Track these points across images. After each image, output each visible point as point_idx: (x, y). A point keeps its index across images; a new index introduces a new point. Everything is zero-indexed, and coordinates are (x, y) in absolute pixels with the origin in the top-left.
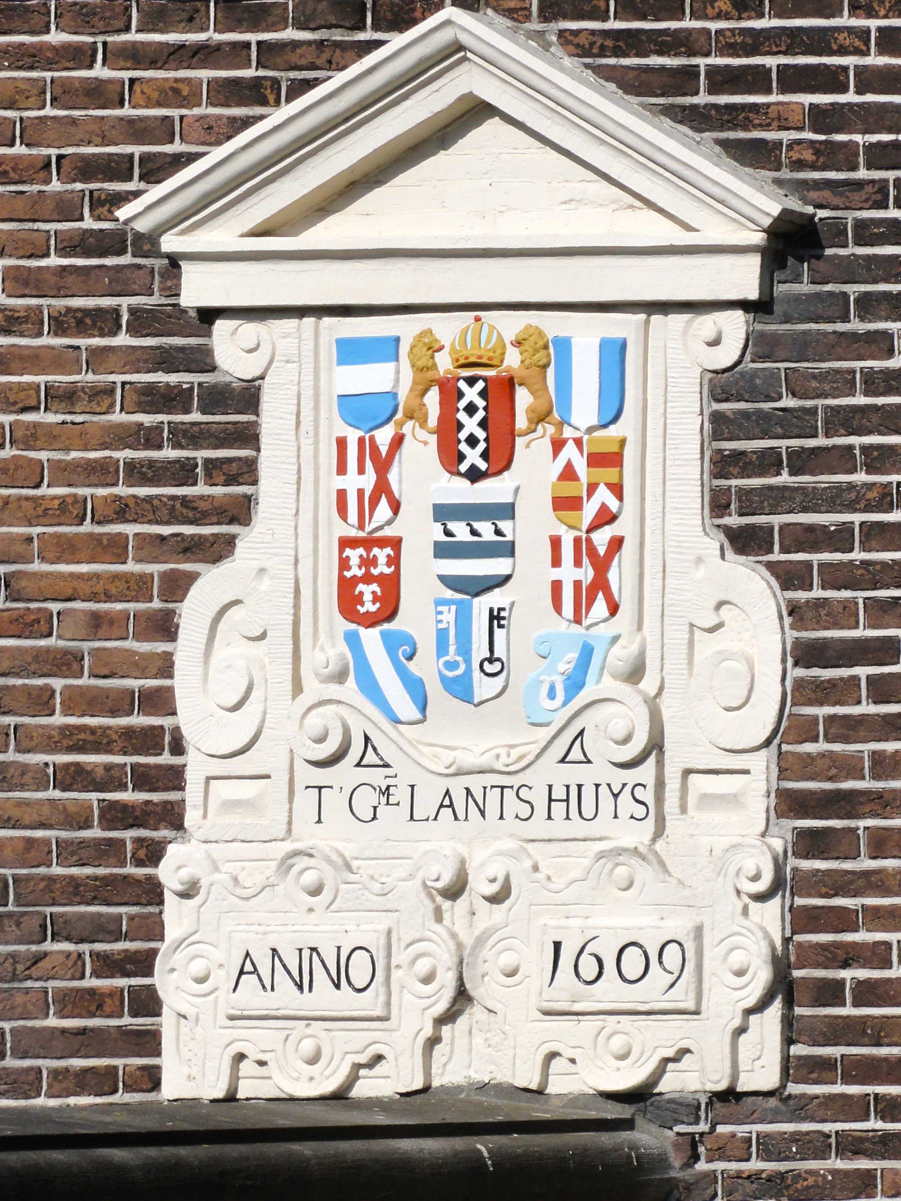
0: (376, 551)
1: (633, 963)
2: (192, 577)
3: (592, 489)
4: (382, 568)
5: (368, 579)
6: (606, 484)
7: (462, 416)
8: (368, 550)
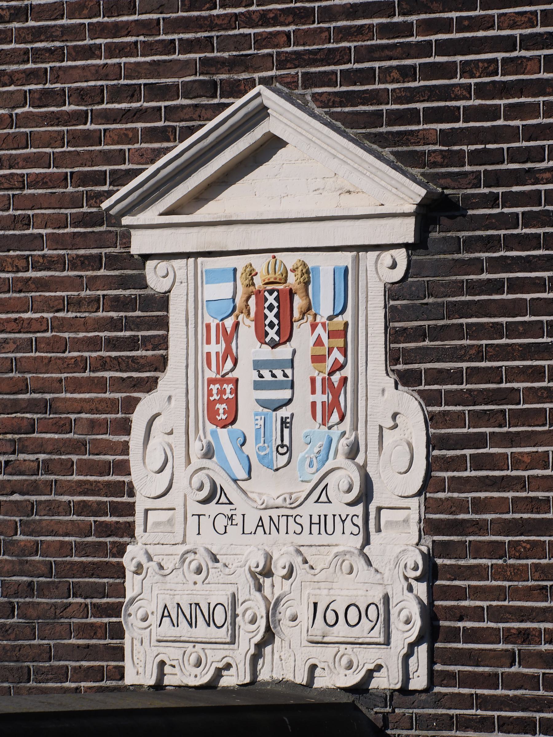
0: (225, 386)
1: (353, 614)
2: (138, 400)
3: (330, 350)
4: (228, 395)
5: (221, 401)
6: (337, 348)
7: (267, 329)
8: (222, 386)
